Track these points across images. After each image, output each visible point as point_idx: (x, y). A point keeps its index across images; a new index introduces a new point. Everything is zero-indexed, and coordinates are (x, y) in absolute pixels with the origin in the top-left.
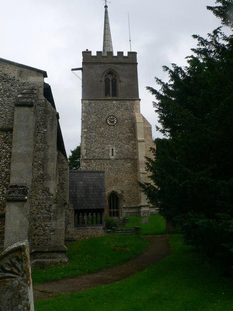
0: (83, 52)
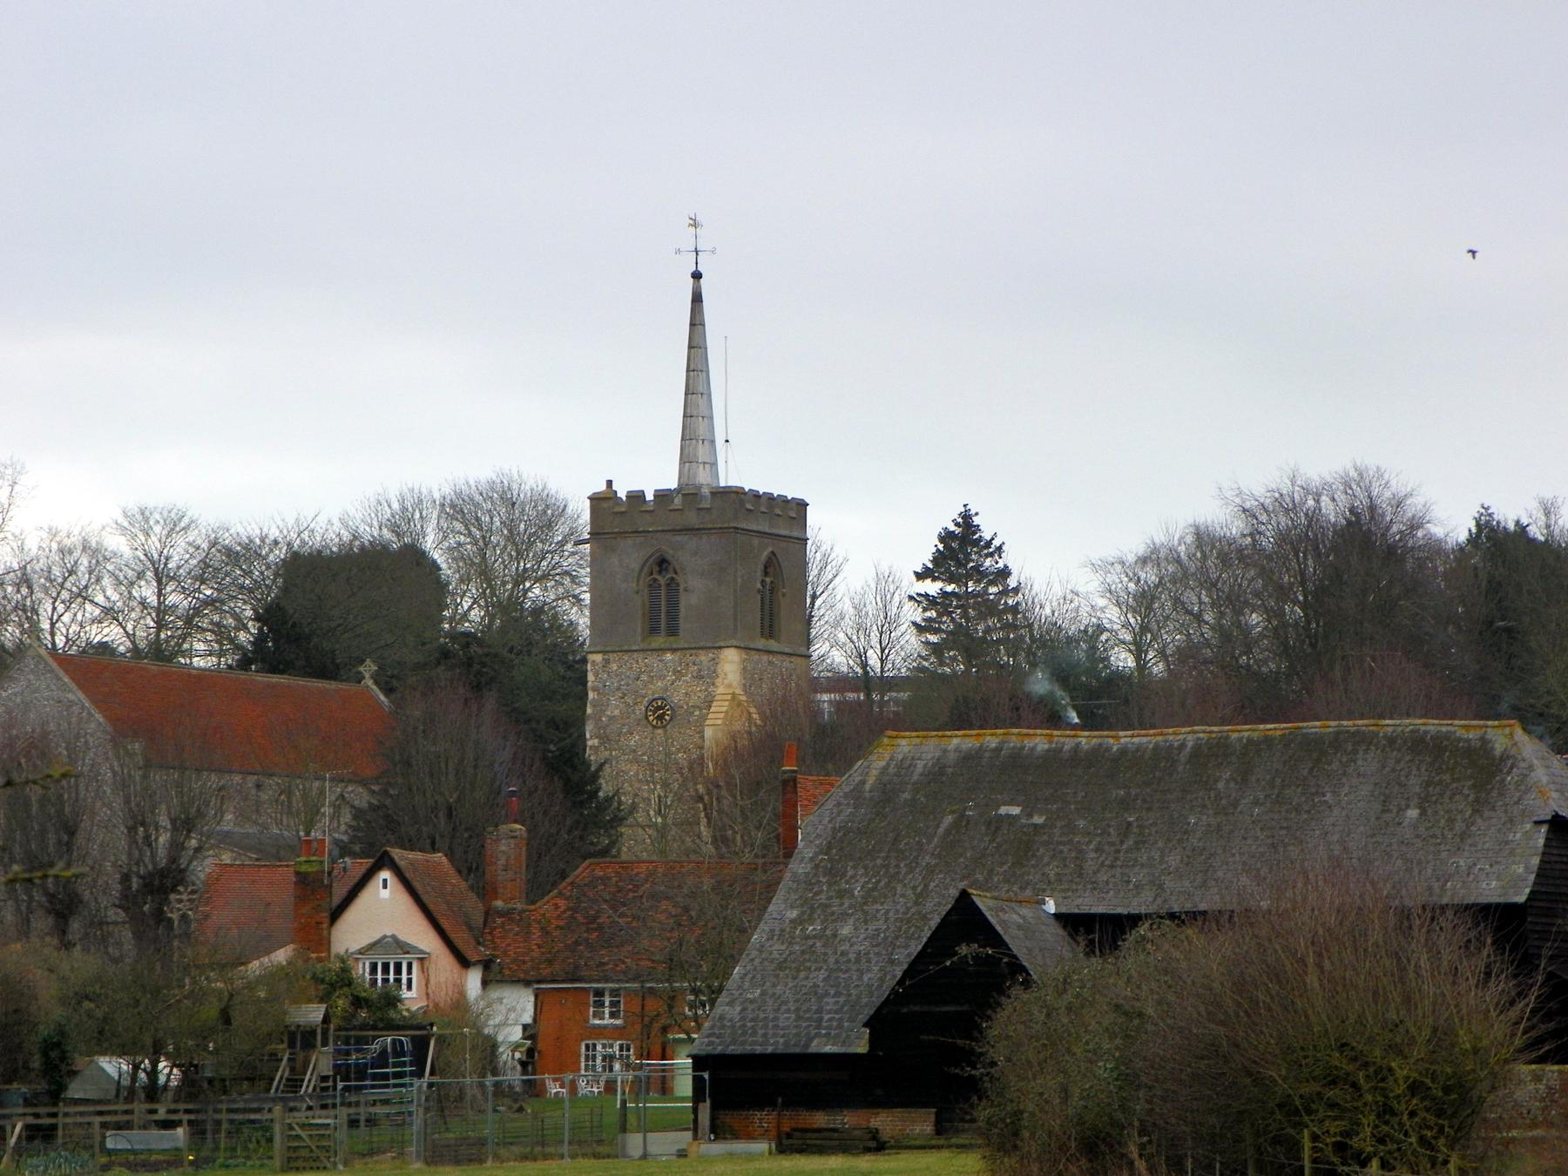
0: (802, 506)
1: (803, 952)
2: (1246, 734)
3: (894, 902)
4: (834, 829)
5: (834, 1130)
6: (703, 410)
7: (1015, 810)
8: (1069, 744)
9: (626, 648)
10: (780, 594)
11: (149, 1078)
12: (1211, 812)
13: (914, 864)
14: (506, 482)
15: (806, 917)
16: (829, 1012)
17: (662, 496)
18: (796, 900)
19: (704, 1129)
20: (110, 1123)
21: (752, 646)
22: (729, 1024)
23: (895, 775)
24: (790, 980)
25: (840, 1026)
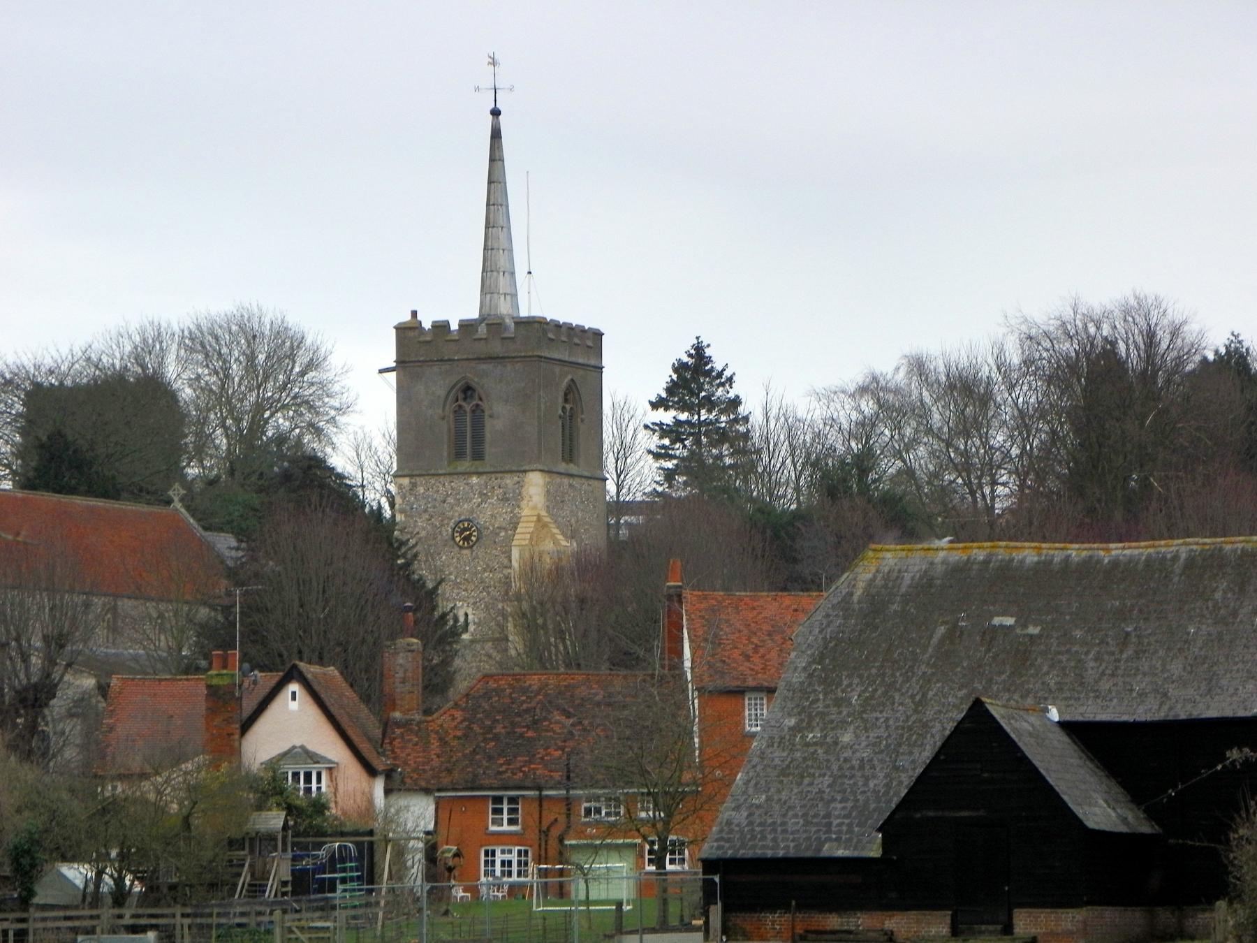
0: (598, 335)
1: (805, 759)
2: (1240, 546)
3: (893, 710)
4: (824, 638)
5: (849, 932)
6: (503, 243)
7: (1009, 621)
8: (1058, 556)
9: (433, 472)
10: (579, 420)
11: (116, 884)
12: (1210, 621)
13: (910, 674)
14: (246, 316)
15: (804, 724)
16: (838, 817)
17: (466, 326)
18: (793, 708)
19: (715, 930)
20: (79, 928)
21: (554, 470)
22: (737, 829)
23: (883, 587)
24: (794, 786)
25: (850, 831)
